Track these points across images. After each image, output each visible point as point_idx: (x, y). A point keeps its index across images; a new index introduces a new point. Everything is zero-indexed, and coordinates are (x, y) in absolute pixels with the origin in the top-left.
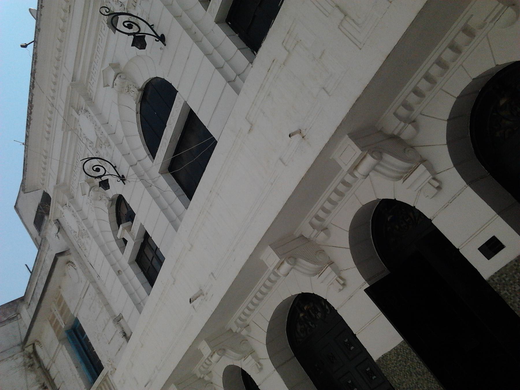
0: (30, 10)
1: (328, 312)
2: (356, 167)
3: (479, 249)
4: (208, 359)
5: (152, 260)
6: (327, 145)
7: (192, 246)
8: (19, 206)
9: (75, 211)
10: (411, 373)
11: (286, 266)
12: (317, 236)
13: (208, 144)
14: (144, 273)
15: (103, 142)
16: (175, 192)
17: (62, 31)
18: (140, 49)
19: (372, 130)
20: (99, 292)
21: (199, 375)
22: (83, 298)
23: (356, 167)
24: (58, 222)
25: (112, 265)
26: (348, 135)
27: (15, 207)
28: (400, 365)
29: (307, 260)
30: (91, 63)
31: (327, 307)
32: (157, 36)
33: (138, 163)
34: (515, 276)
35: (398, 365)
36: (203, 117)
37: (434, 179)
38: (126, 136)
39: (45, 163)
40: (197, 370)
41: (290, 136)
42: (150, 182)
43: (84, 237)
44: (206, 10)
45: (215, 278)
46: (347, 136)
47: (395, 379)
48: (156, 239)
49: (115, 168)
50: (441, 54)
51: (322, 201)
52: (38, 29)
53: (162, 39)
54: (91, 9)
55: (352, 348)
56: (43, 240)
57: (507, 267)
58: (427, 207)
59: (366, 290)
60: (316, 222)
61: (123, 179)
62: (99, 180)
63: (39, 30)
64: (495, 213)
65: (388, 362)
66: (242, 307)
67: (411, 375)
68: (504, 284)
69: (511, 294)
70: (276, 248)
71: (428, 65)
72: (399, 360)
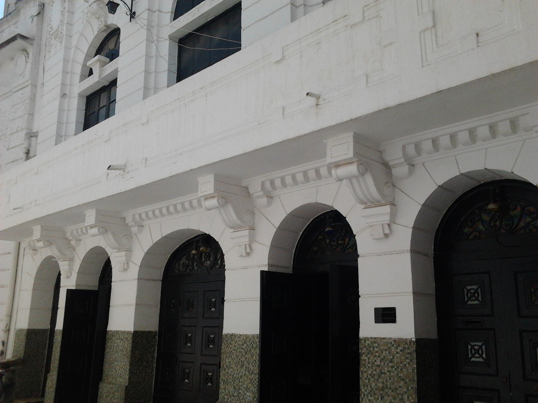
1: (217, 267)
2: (338, 165)
3: (375, 309)
4: (86, 227)
5: (102, 108)
7: (148, 122)
9: (66, 9)
10: (243, 365)
11: (214, 202)
12: (258, 197)
13: (231, 45)
14: (86, 113)
16: (169, 65)
19: (374, 145)
20: (33, 99)
21: (68, 235)
22: (15, 92)
23: (338, 165)
25: (62, 84)
26: (354, 133)
28: (240, 352)
29: (237, 213)
31: (219, 262)
33: (157, 12)
34: (384, 352)
35: (238, 350)
37: (389, 225)
40: (70, 230)
41: (308, 94)
42: (155, 38)
43: (57, 39)
45: (146, 164)
46: (352, 133)
47: (227, 360)
48: (120, 92)
50: (479, 126)
51: (287, 172)
55: (213, 309)
56: (16, 12)
57: (384, 340)
58: (364, 243)
59: (262, 272)
60: (268, 185)
61: (133, 15)
64: (412, 290)
65: (232, 343)
66: (149, 208)
67: (242, 367)
68: (370, 351)
69: (369, 363)
70: (218, 180)
71: (461, 128)
72: (243, 347)
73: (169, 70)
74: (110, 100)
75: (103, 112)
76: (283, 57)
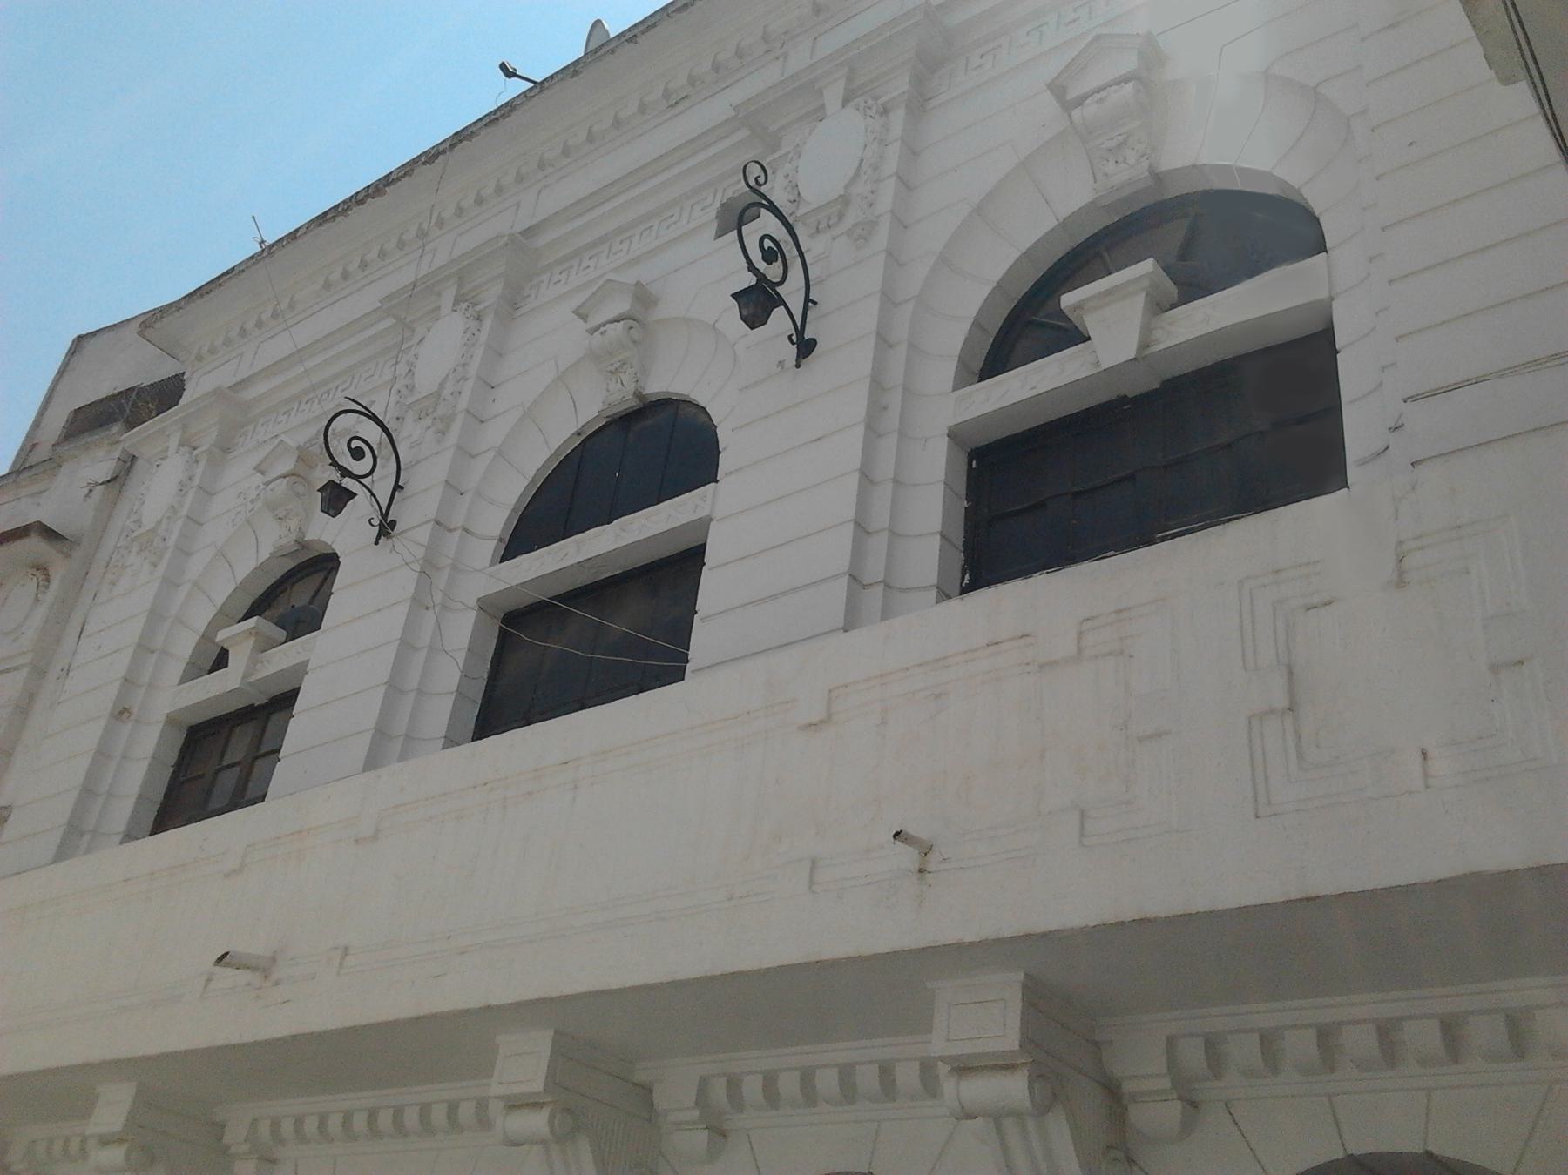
0: (598, 23)
2: (964, 1068)
5: (229, 766)
6: (959, 948)
7: (375, 837)
8: (90, 346)
9: (196, 481)
11: (536, 1122)
13: (656, 659)
14: (175, 776)
15: (440, 411)
17: (617, 123)
18: (744, 319)
23: (964, 1068)
24: (129, 463)
27: (80, 337)
30: (603, 240)
32: (800, 331)
36: (712, 589)
38: (500, 453)
39: (259, 324)
41: (897, 835)
42: (438, 598)
44: (954, 389)
45: (341, 965)
46: (1021, 976)
48: (299, 730)
49: (397, 487)
50: (1410, 1017)
52: (573, 70)
53: (805, 347)
54: (721, 146)
60: (719, 1092)
61: (386, 528)
62: (335, 476)
63: (576, 73)
73: (460, 694)
74: (258, 748)
75: (228, 780)
76: (830, 716)
